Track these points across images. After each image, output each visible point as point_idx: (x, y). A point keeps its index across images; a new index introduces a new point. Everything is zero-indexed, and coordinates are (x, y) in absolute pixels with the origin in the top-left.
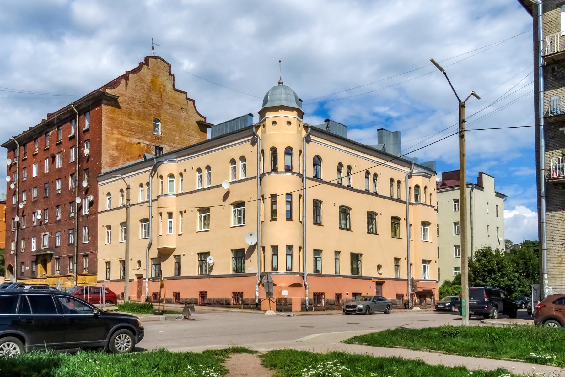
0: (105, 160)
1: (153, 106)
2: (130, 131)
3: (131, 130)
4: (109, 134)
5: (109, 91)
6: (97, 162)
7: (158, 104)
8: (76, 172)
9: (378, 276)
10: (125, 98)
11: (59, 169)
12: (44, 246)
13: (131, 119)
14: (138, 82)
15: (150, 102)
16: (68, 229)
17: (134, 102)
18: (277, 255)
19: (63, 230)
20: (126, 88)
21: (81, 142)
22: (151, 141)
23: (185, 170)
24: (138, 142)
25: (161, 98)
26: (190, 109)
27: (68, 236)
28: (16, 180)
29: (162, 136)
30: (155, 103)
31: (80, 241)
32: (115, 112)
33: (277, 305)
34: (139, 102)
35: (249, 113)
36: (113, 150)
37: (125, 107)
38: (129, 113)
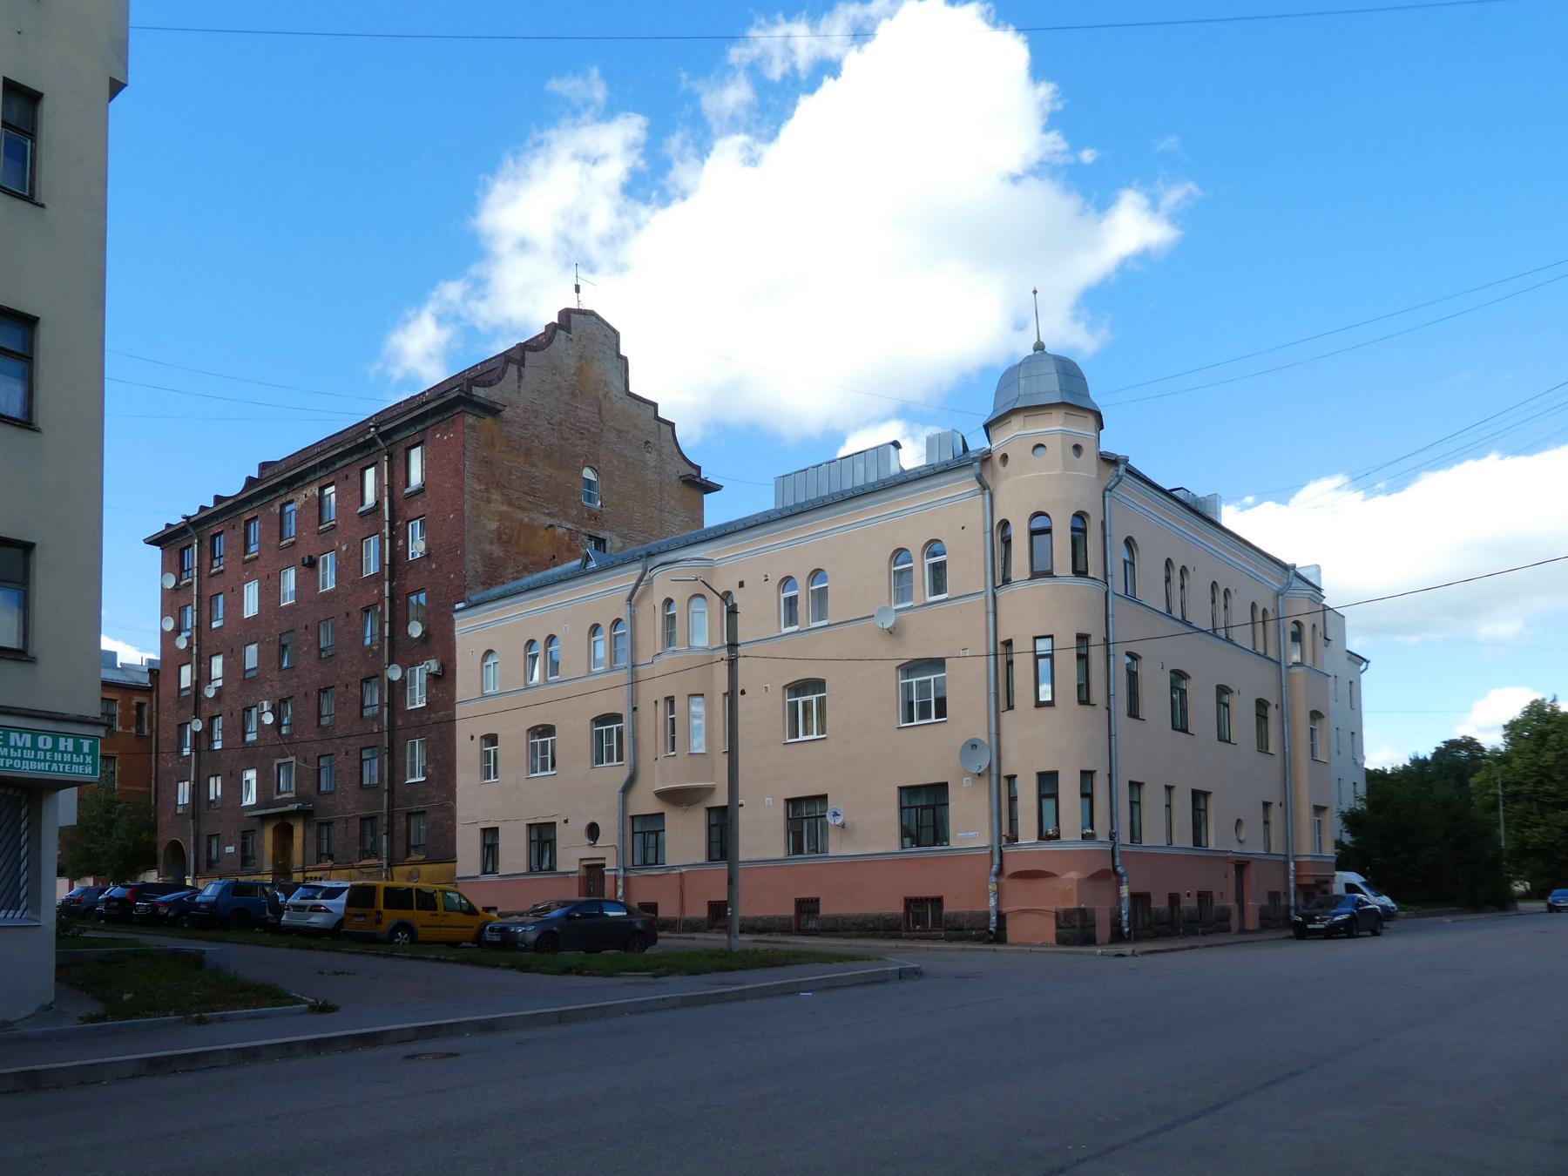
1: (582, 433)
5: (479, 392)
9: (1236, 848)
10: (518, 411)
12: (279, 792)
13: (533, 465)
14: (545, 373)
18: (1055, 796)
20: (519, 387)
22: (577, 523)
23: (741, 584)
24: (548, 523)
27: (358, 765)
28: (189, 626)
30: (587, 426)
33: (1058, 927)
35: (892, 440)
36: (491, 543)
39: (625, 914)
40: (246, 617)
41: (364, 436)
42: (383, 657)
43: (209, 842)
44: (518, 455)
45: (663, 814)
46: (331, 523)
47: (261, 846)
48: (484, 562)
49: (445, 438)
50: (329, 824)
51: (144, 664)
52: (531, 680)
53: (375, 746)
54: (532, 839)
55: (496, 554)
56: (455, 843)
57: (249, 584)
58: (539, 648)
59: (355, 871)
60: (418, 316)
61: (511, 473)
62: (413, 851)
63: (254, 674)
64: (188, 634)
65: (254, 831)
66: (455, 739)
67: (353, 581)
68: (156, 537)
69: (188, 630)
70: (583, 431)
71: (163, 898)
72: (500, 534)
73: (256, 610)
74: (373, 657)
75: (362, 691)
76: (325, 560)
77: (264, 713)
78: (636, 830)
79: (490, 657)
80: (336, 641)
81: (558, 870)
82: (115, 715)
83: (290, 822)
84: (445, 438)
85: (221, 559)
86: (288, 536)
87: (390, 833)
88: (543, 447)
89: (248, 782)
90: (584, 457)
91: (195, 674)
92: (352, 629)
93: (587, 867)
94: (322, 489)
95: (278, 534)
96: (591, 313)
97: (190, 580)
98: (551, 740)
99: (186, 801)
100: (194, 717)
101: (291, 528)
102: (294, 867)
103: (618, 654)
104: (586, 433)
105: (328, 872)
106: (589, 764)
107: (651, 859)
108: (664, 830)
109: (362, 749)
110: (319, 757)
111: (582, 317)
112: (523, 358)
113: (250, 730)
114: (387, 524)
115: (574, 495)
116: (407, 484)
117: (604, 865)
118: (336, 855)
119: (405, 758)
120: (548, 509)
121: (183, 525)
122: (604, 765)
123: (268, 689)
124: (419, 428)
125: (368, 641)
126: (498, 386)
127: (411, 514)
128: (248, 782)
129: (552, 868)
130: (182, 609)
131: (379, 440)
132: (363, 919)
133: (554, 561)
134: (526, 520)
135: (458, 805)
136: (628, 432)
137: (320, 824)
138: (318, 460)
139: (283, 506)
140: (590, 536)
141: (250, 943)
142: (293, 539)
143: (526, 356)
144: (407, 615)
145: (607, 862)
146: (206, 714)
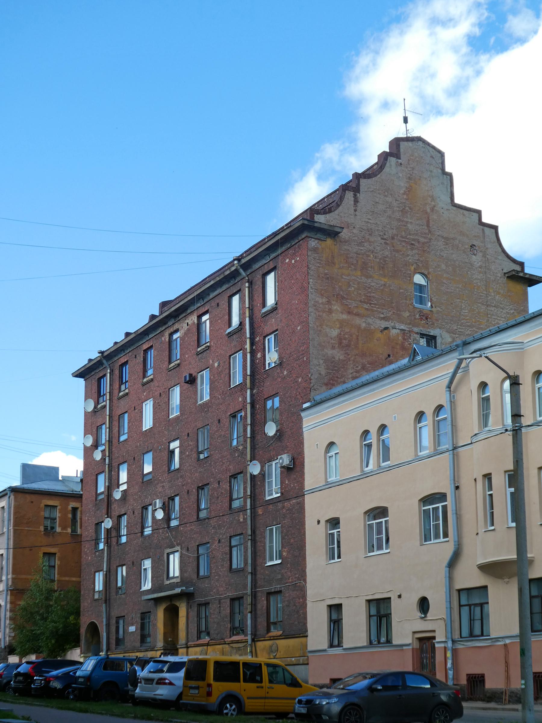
0: (318, 370)
1: (412, 244)
2: (367, 303)
3: (368, 300)
4: (324, 312)
5: (320, 219)
6: (298, 377)
7: (422, 240)
8: (244, 408)
10: (355, 231)
11: (206, 404)
13: (368, 277)
14: (378, 196)
15: (406, 237)
16: (228, 535)
17: (372, 239)
19: (216, 539)
20: (355, 210)
21: (257, 339)
22: (410, 324)
24: (383, 326)
25: (428, 226)
26: (489, 246)
27: (228, 551)
28: (103, 442)
29: (434, 309)
30: (416, 237)
31: (259, 561)
32: (334, 264)
34: (382, 239)
36: (333, 348)
37: (355, 250)
38: (364, 263)
39: (429, 686)
40: (144, 430)
41: (229, 268)
42: (246, 455)
43: (117, 623)
44: (355, 269)
45: (485, 587)
46: (206, 345)
47: (155, 625)
48: (327, 365)
49: (293, 261)
50: (206, 604)
51: (79, 475)
52: (367, 466)
53: (242, 534)
54: (372, 614)
55: (337, 358)
56: (305, 618)
57: (146, 403)
58: (373, 439)
59: (227, 646)
60: (304, 174)
61: (349, 286)
62: (272, 627)
63: (150, 477)
64: (103, 447)
65: (150, 612)
66: (305, 524)
67: (223, 391)
68: (81, 371)
69: (103, 445)
70: (413, 242)
71: (54, 673)
72: (340, 339)
73: (152, 424)
74: (239, 456)
75: (230, 486)
76: (202, 377)
77: (156, 510)
78: (463, 602)
79: (332, 449)
80: (211, 444)
81: (395, 642)
82: (56, 519)
83: (175, 604)
84: (293, 261)
85: (127, 384)
86: (175, 359)
87: (254, 611)
88: (378, 260)
89: (145, 569)
90: (415, 265)
91: (107, 481)
92: (223, 433)
93: (420, 639)
94: (200, 317)
95: (167, 359)
96: (419, 139)
97: (104, 403)
98: (385, 521)
99: (101, 589)
100: (106, 516)
101: (177, 353)
102: (180, 643)
103: (441, 437)
104: (416, 244)
105: (205, 647)
106: (419, 542)
107: (477, 631)
108: (488, 603)
109: (231, 537)
110: (198, 546)
111: (410, 144)
112: (358, 185)
113: (147, 525)
114: (248, 341)
115: (406, 299)
116: (264, 305)
117: (434, 638)
118: (212, 632)
119: (265, 543)
120: (383, 314)
121: (99, 359)
122: (432, 542)
123: (160, 489)
124: (273, 256)
125: (235, 443)
126: (336, 212)
127: (267, 329)
128: (145, 569)
129: (389, 641)
130: (99, 428)
131: (241, 271)
132: (197, 691)
133: (389, 359)
134: (364, 325)
135: (308, 585)
136: (454, 239)
137: (200, 605)
138: (196, 294)
139: (171, 335)
140: (421, 334)
141: (106, 714)
142: (178, 361)
143: (361, 184)
144: (265, 417)
145: (437, 634)
146: (115, 514)
